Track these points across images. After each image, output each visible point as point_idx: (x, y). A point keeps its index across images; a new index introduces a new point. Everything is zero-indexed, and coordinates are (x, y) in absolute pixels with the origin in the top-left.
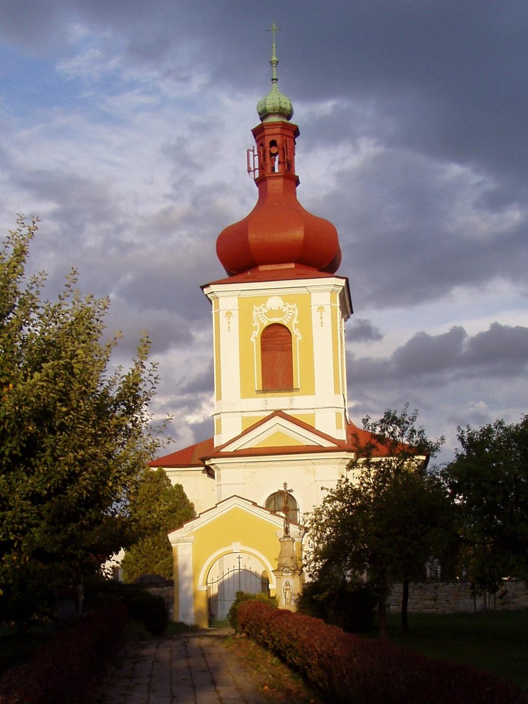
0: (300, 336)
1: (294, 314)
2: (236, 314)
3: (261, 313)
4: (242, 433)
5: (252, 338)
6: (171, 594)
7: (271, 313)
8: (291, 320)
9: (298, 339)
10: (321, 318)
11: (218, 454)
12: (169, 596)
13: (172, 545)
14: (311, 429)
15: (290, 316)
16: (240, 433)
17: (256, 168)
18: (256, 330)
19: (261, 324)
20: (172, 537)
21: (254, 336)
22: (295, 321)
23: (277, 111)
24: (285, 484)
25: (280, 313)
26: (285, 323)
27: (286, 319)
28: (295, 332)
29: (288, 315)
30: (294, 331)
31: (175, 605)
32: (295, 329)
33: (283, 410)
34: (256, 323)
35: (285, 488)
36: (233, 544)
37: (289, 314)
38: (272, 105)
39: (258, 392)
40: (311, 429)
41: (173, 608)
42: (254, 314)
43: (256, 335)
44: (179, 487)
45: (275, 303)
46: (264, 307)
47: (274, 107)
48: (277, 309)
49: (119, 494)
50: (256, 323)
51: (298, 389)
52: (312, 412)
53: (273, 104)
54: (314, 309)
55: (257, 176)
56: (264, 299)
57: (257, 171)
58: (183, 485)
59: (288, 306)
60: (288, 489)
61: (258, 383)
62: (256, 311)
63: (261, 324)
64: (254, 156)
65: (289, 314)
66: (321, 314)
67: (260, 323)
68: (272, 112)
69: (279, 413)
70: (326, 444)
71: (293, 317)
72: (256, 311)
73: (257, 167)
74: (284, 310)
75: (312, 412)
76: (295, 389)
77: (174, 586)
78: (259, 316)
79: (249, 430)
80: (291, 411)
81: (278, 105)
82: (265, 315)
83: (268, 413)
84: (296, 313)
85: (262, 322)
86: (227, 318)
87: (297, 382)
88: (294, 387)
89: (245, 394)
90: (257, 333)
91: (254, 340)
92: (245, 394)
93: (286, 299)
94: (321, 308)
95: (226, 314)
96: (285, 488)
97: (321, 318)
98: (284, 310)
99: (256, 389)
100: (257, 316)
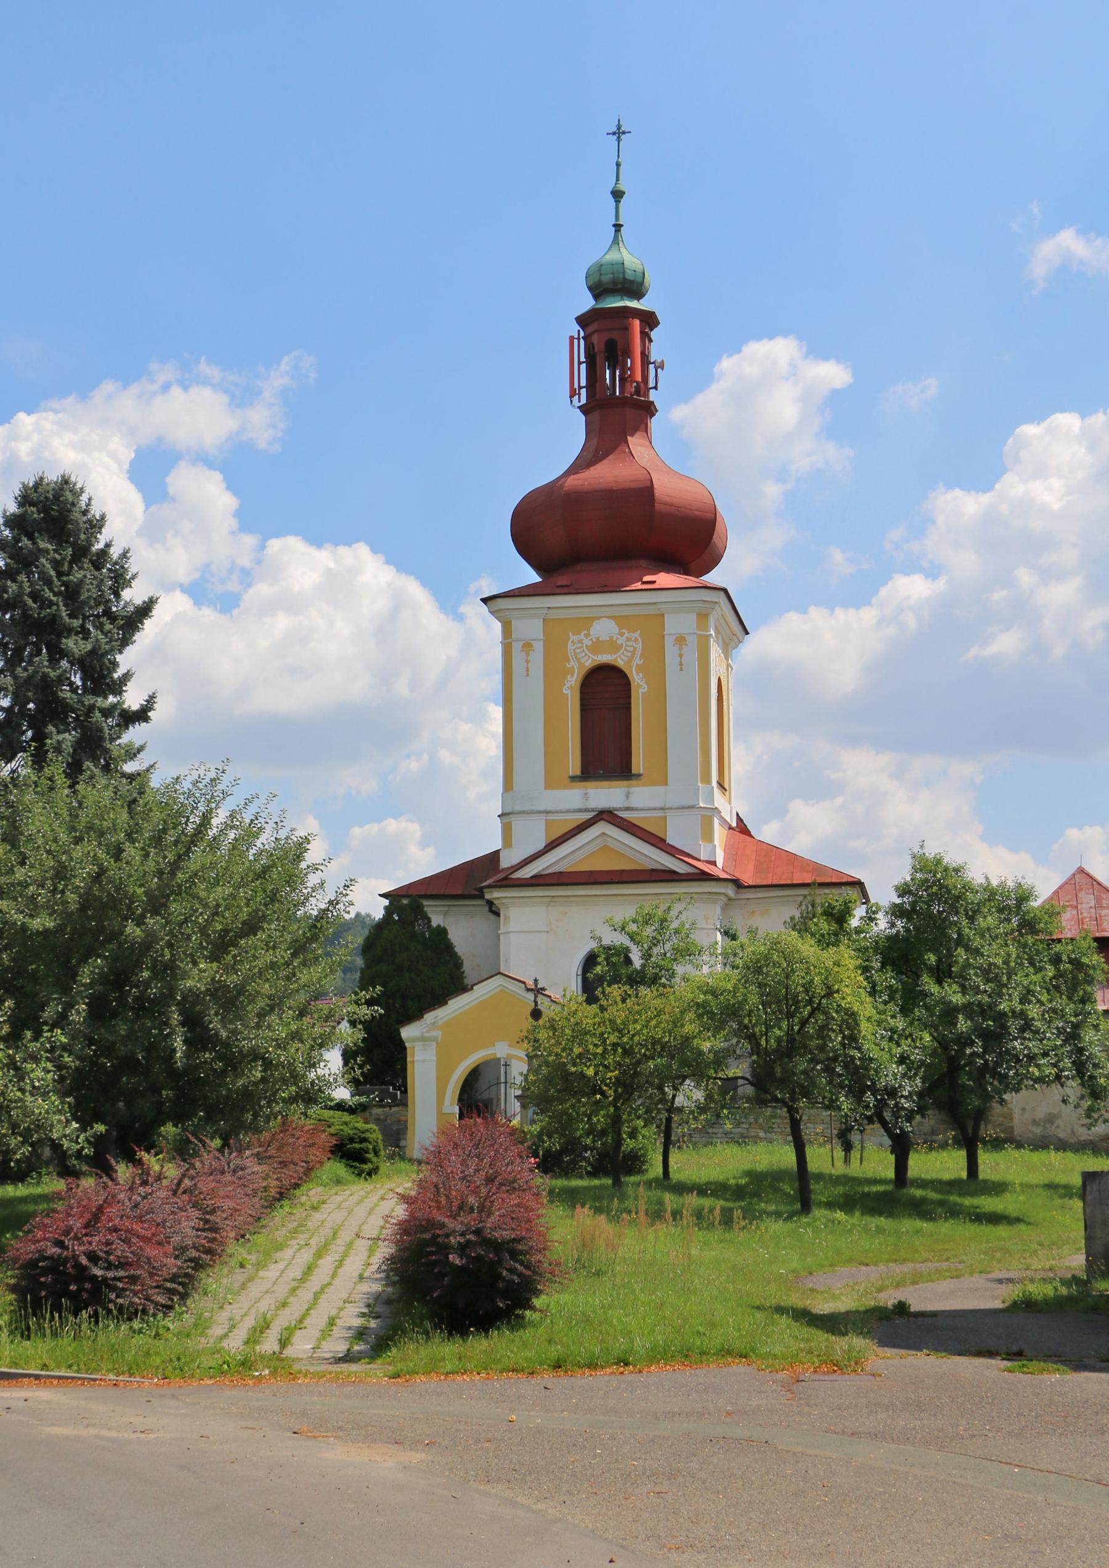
0: (644, 685)
1: (635, 649)
2: (538, 647)
3: (580, 645)
4: (545, 847)
5: (566, 687)
6: (403, 1118)
7: (597, 646)
8: (631, 659)
9: (641, 691)
10: (681, 656)
11: (508, 882)
12: (399, 1121)
13: (407, 1045)
14: (658, 842)
15: (627, 651)
16: (541, 845)
17: (582, 385)
18: (572, 676)
19: (581, 665)
20: (407, 1033)
21: (568, 685)
22: (637, 661)
23: (620, 286)
24: (536, 980)
25: (612, 646)
26: (620, 663)
27: (623, 657)
28: (637, 679)
29: (625, 650)
30: (635, 677)
31: (409, 1132)
32: (637, 674)
33: (620, 809)
34: (573, 664)
35: (536, 986)
36: (496, 1044)
37: (628, 648)
38: (611, 276)
39: (573, 778)
40: (658, 842)
41: (406, 1139)
42: (570, 647)
43: (571, 687)
44: (442, 932)
45: (604, 629)
46: (587, 636)
47: (614, 278)
48: (608, 639)
49: (211, 1165)
50: (573, 664)
51: (639, 776)
52: (660, 814)
53: (613, 273)
54: (669, 642)
55: (584, 401)
56: (588, 621)
57: (584, 392)
58: (447, 928)
59: (627, 635)
60: (539, 986)
61: (574, 765)
62: (573, 642)
63: (581, 665)
64: (580, 363)
65: (628, 648)
66: (681, 649)
67: (579, 663)
68: (610, 287)
69: (606, 815)
70: (680, 868)
71: (633, 653)
72: (573, 642)
73: (583, 383)
74: (619, 642)
75: (660, 814)
76: (634, 775)
77: (407, 1106)
78: (578, 651)
79: (554, 845)
80: (629, 812)
81: (621, 276)
82: (589, 651)
83: (588, 816)
84: (639, 646)
85: (582, 661)
86: (524, 654)
87: (639, 763)
88: (633, 772)
89: (550, 783)
90: (574, 679)
91: (569, 692)
92: (550, 783)
93: (622, 621)
94: (681, 640)
95: (523, 647)
96: (536, 986)
97: (681, 656)
98: (619, 642)
99: (571, 774)
100: (574, 650)
